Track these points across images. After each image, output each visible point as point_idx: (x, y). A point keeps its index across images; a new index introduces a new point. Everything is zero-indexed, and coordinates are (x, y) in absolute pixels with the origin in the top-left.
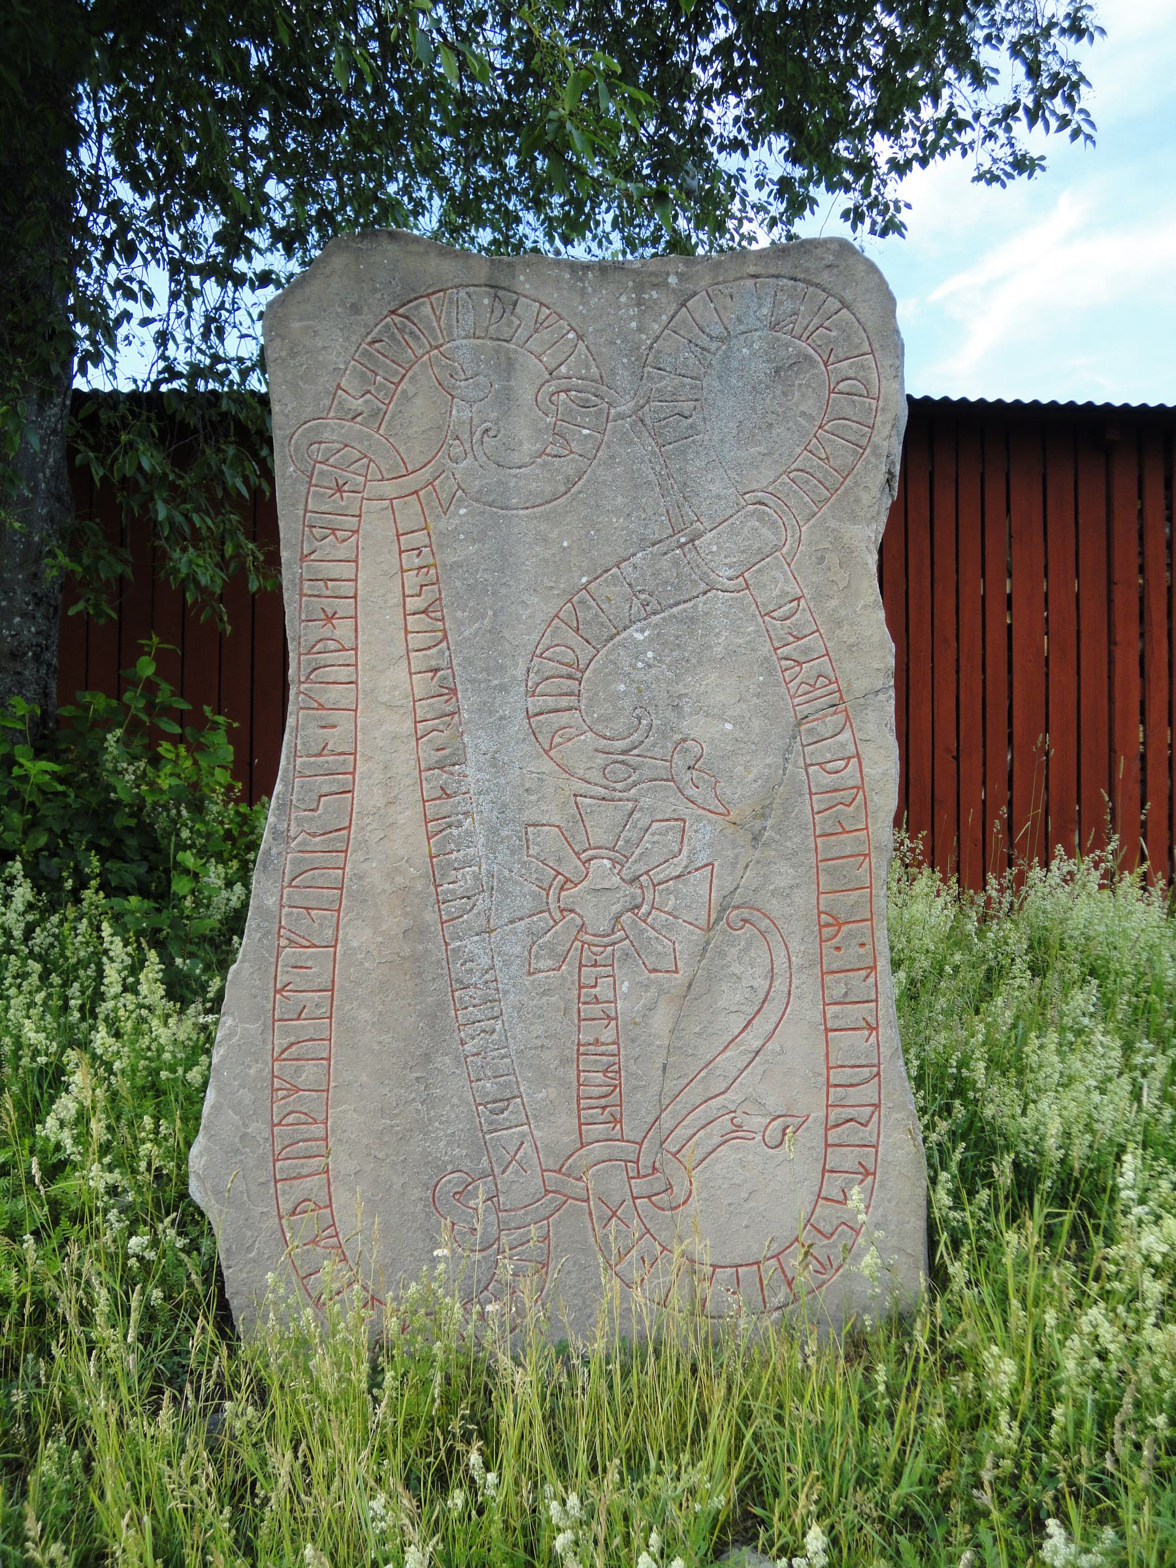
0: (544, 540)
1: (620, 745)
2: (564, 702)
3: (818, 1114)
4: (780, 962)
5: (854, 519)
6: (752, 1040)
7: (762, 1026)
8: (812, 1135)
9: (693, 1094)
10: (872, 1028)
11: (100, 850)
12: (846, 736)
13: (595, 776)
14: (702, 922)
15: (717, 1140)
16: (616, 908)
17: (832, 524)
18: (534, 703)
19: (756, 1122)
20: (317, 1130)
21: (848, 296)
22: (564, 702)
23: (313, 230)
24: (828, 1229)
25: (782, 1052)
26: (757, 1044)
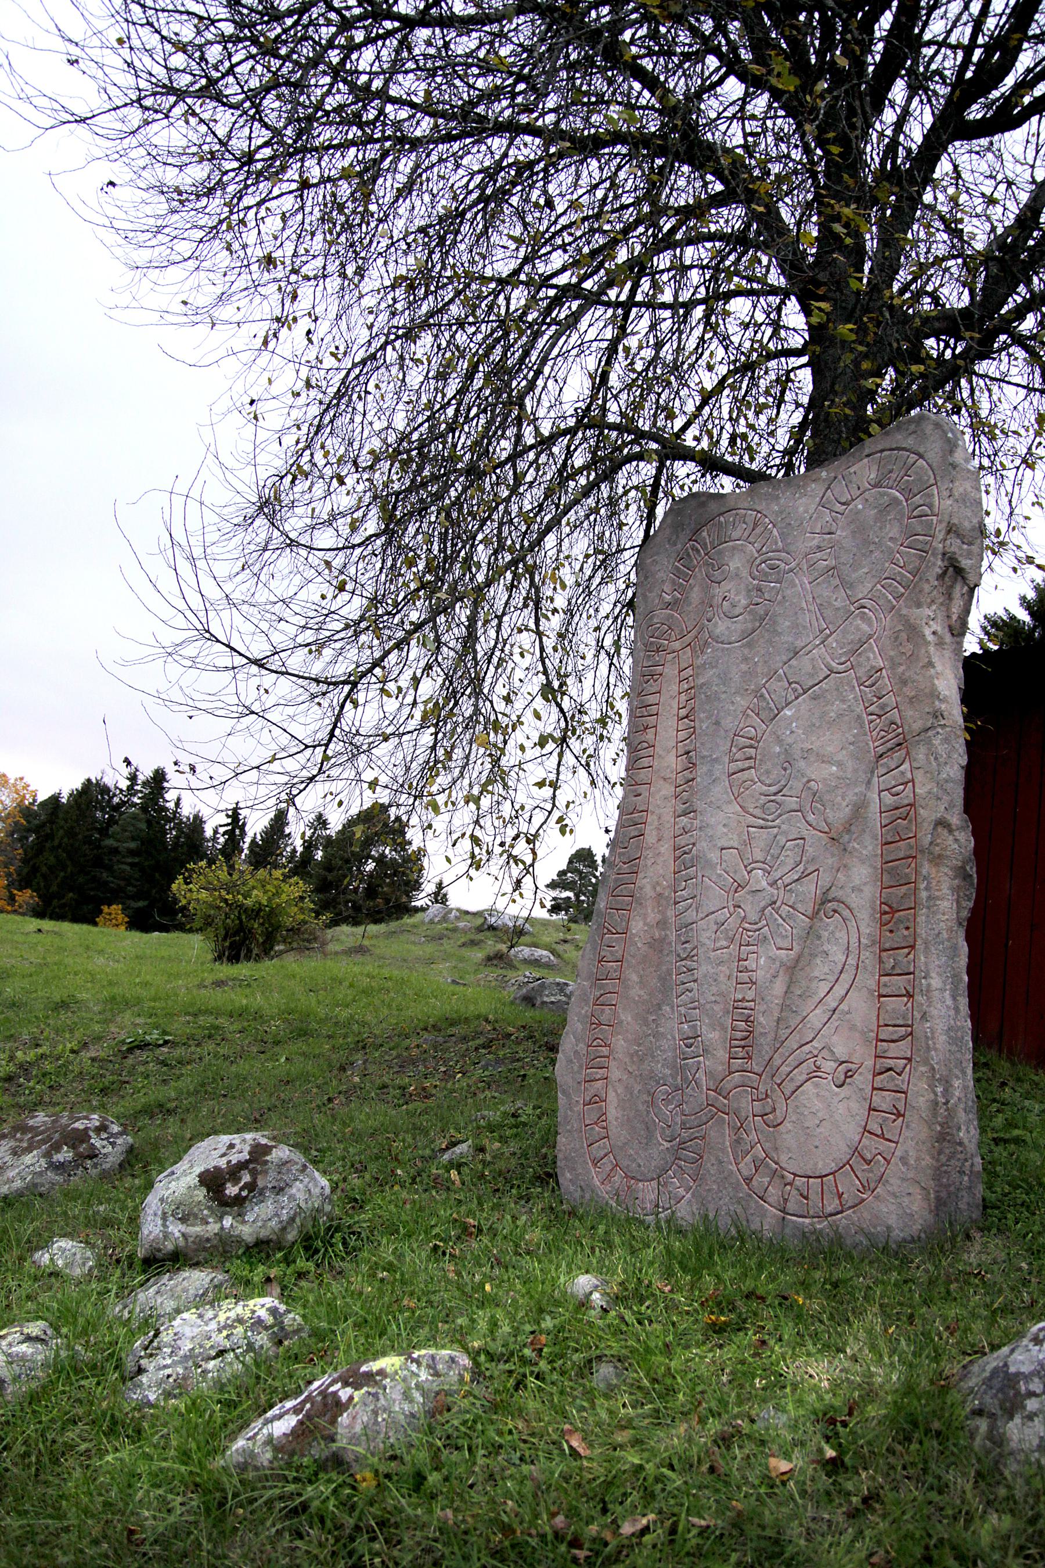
0: (746, 659)
1: (773, 789)
2: (747, 764)
3: (869, 1063)
4: (854, 940)
5: (919, 605)
6: (831, 1002)
7: (839, 990)
8: (863, 1079)
9: (792, 1043)
10: (910, 995)
11: (151, 1405)
12: (906, 766)
13: (758, 812)
14: (809, 913)
15: (805, 1077)
16: (763, 904)
17: (904, 611)
18: (734, 766)
19: (829, 1066)
20: (605, 1051)
21: (921, 450)
22: (747, 764)
23: (44, 1258)
24: (869, 1157)
25: (849, 1012)
26: (834, 1005)
